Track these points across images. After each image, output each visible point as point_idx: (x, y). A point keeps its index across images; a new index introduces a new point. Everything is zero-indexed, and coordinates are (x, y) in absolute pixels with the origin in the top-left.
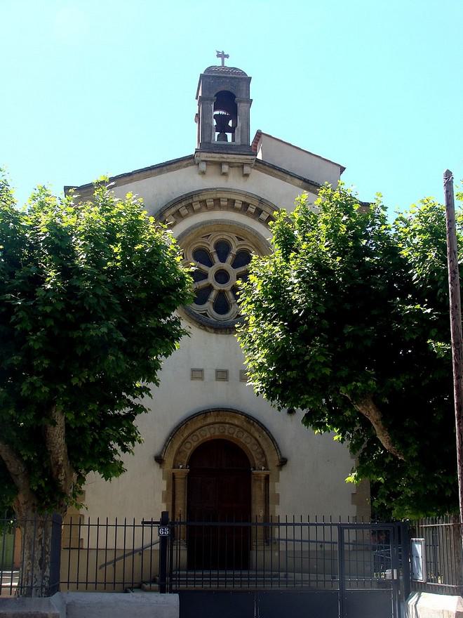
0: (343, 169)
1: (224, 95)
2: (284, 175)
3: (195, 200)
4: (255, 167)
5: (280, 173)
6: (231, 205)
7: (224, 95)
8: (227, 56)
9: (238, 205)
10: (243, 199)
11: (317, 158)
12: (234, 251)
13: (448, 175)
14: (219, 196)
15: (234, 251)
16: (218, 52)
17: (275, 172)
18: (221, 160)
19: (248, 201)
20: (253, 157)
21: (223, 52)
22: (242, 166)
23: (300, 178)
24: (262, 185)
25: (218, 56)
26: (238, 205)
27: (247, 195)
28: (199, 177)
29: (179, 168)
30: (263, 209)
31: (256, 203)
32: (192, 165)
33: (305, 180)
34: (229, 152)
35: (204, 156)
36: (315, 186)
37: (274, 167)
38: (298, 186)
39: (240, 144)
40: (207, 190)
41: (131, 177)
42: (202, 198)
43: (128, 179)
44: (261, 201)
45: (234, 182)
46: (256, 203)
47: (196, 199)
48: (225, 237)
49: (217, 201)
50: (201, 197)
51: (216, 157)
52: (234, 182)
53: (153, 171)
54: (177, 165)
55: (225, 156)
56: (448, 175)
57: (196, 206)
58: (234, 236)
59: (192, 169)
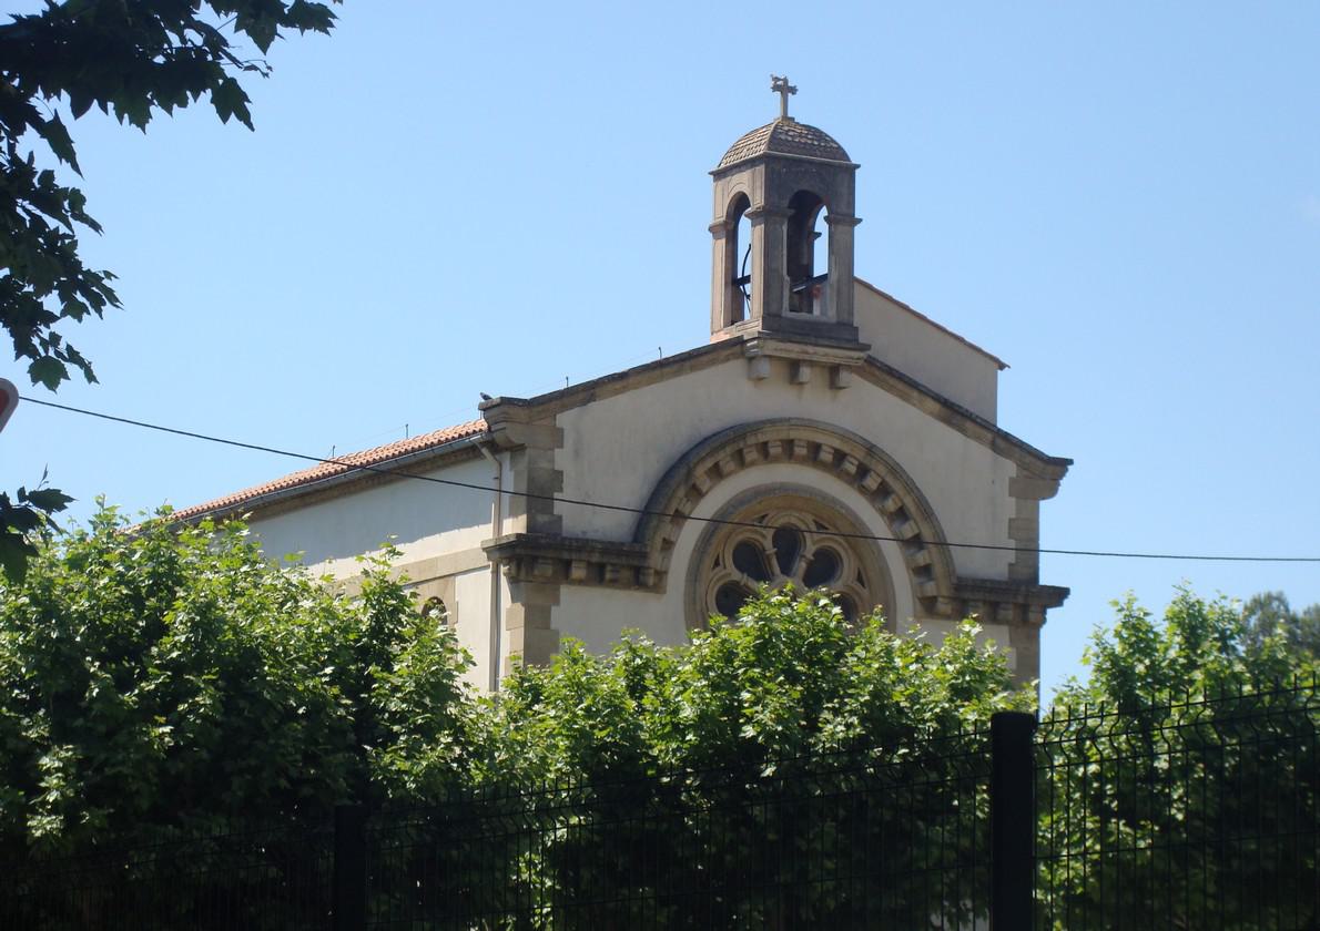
0: (1002, 366)
1: (800, 184)
2: (907, 390)
3: (749, 443)
4: (859, 371)
5: (900, 386)
6: (813, 454)
7: (800, 184)
8: (793, 90)
9: (826, 456)
10: (837, 444)
11: (957, 342)
12: (810, 548)
13: (253, 130)
14: (793, 434)
15: (810, 548)
16: (776, 79)
17: (892, 381)
18: (801, 357)
19: (845, 448)
20: (862, 354)
21: (785, 81)
22: (834, 370)
23: (937, 398)
24: (865, 411)
25: (776, 88)
26: (826, 456)
27: (845, 436)
28: (747, 387)
29: (713, 363)
30: (873, 467)
31: (860, 454)
32: (738, 358)
33: (946, 403)
34: (821, 341)
35: (772, 347)
36: (962, 415)
37: (891, 372)
38: (931, 414)
39: (834, 320)
40: (773, 422)
41: (624, 383)
42: (762, 438)
43: (618, 385)
44: (871, 449)
45: (812, 404)
46: (860, 454)
47: (751, 440)
48: (793, 521)
49: (789, 445)
50: (759, 436)
51: (794, 350)
52: (812, 404)
53: (666, 370)
54: (710, 356)
55: (810, 349)
56: (253, 130)
57: (751, 455)
58: (809, 518)
59: (736, 367)
